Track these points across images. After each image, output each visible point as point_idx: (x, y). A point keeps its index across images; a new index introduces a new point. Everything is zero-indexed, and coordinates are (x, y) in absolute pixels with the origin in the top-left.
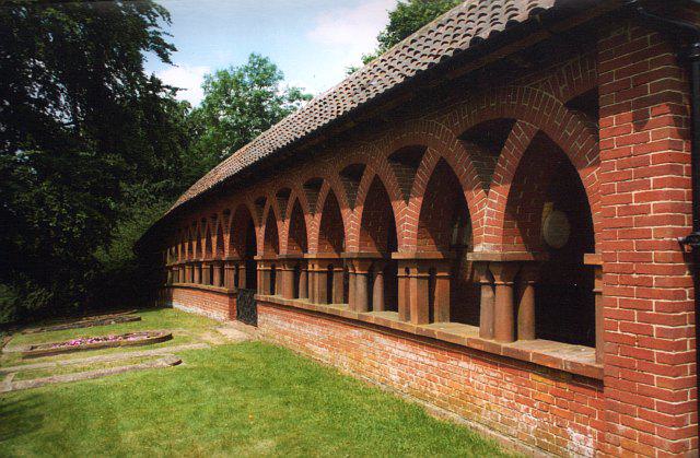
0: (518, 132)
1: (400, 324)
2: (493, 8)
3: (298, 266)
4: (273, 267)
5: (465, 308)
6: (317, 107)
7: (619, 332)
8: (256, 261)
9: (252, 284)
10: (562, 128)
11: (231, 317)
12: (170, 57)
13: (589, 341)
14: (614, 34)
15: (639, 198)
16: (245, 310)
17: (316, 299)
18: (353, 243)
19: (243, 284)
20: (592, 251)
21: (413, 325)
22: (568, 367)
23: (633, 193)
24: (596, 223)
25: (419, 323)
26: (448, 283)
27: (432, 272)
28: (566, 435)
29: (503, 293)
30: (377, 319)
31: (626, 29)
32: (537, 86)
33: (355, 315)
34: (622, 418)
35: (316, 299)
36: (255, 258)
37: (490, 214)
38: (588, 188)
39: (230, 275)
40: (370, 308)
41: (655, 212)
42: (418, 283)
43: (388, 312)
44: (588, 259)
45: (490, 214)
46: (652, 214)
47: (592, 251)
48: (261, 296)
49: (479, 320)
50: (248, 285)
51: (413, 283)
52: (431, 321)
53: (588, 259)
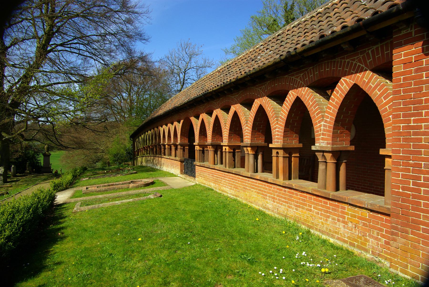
0: (342, 84)
1: (274, 180)
2: (305, 33)
3: (217, 148)
4: (203, 148)
5: (267, 167)
6: (226, 68)
7: (401, 190)
8: (195, 145)
9: (192, 156)
10: (369, 82)
11: (182, 172)
12: (66, 234)
13: (381, 193)
14: (404, 32)
15: (415, 121)
16: (189, 169)
17: (227, 166)
18: (210, 139)
19: (187, 156)
20: (384, 147)
21: (227, 169)
22: (369, 206)
23: (412, 118)
24: (386, 133)
25: (284, 180)
26: (298, 159)
27: (290, 154)
28: (367, 240)
29: (331, 168)
30: (236, 172)
31: (411, 29)
32: (354, 60)
33: (249, 174)
34: (401, 235)
35: (227, 166)
36: (194, 144)
37: (324, 126)
38: (383, 114)
39: (179, 152)
40: (256, 171)
41: (424, 129)
42: (283, 159)
43: (350, 191)
44: (382, 152)
45: (324, 126)
46: (423, 130)
47: (384, 147)
48: (197, 163)
49: (384, 192)
50: (189, 157)
51: (281, 159)
52: (290, 179)
53: (382, 152)
